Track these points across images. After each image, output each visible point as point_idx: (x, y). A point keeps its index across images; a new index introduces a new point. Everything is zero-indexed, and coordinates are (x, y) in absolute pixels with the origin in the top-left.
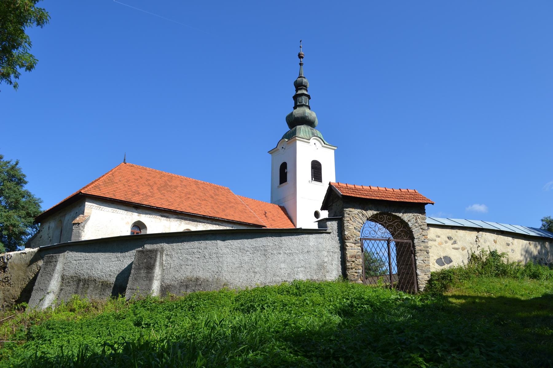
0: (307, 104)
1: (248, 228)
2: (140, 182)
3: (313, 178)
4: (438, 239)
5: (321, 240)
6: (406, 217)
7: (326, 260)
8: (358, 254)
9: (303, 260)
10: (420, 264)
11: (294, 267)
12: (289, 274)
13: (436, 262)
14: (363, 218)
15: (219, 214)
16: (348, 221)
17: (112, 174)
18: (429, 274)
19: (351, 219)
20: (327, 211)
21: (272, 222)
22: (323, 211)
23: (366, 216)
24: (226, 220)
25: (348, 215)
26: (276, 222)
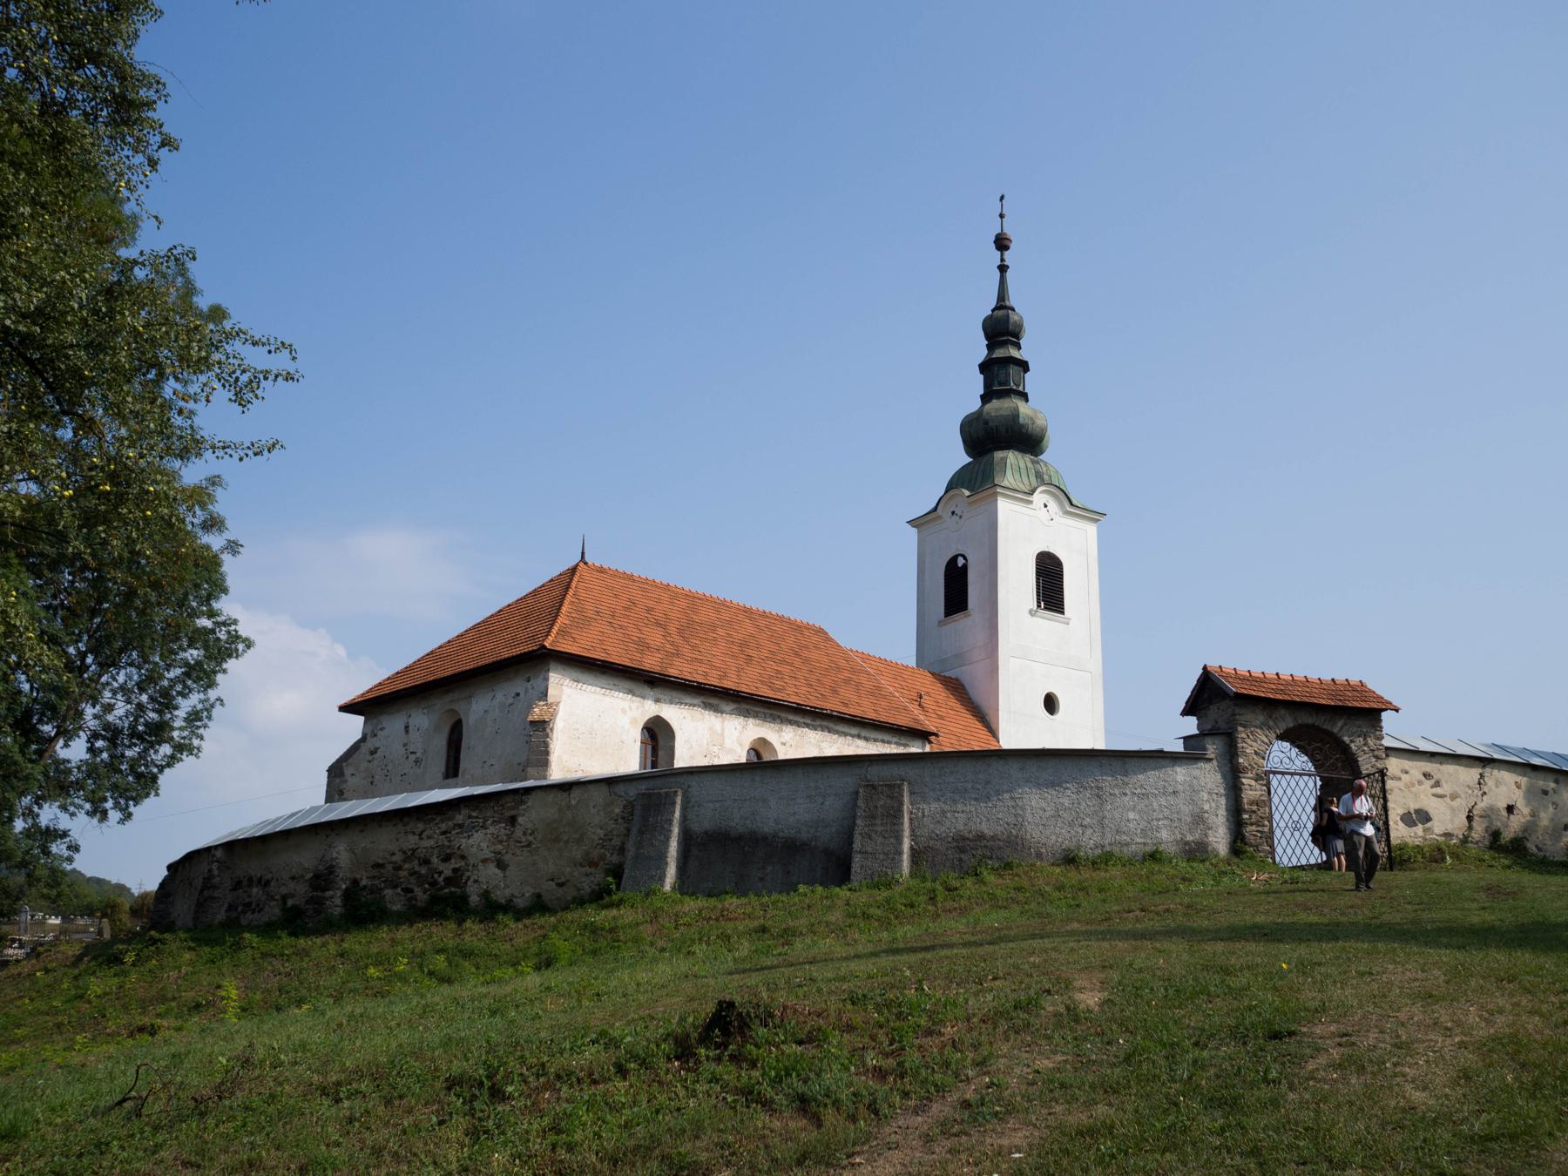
0: (1021, 389)
1: (905, 745)
4: (1404, 776)
5: (1196, 773)
6: (1337, 727)
7: (1206, 807)
8: (1263, 798)
13: (1401, 819)
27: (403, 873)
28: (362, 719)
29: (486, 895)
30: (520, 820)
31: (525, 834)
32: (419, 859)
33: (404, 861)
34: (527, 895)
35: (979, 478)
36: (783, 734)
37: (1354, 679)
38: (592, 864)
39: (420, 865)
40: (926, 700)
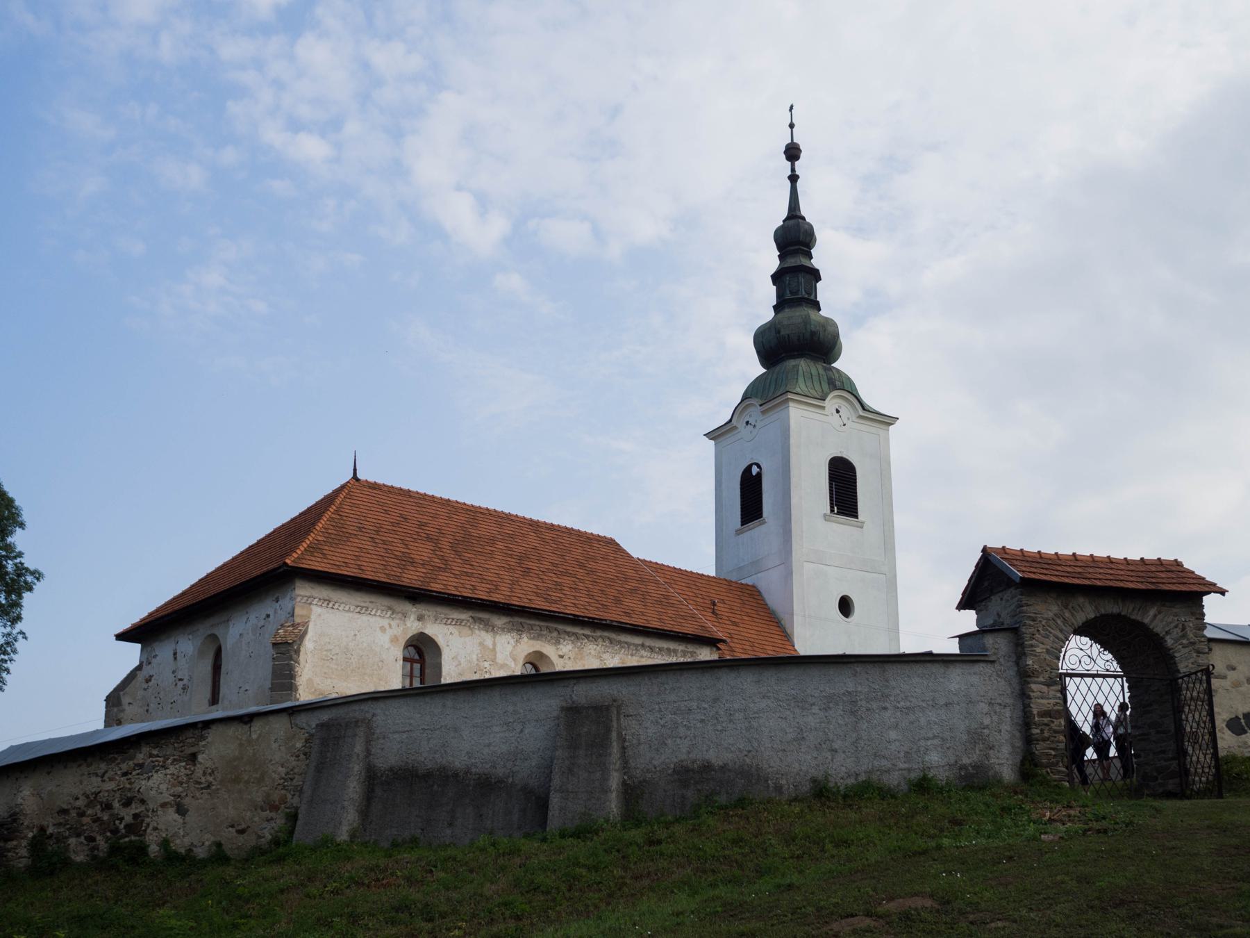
0: (812, 297)
2: (405, 531)
3: (836, 508)
7: (987, 721)
8: (1056, 708)
9: (935, 723)
11: (917, 738)
12: (908, 753)
13: (1227, 726)
14: (1064, 628)
15: (610, 611)
16: (1033, 635)
17: (337, 512)
19: (1038, 631)
20: (973, 612)
21: (732, 627)
22: (961, 611)
23: (1073, 624)
24: (628, 626)
25: (1032, 623)
26: (741, 629)
27: (85, 820)
28: (138, 646)
29: (165, 843)
30: (200, 758)
31: (204, 774)
32: (101, 803)
33: (88, 806)
34: (207, 843)
35: (773, 387)
36: (561, 646)
37: (1168, 556)
38: (274, 808)
39: (103, 810)
40: (720, 607)
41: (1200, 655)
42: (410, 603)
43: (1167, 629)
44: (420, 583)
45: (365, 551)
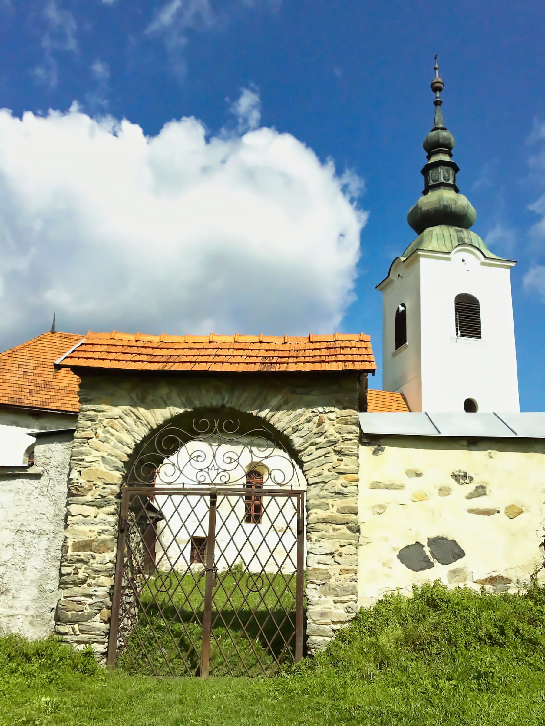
0: (451, 182)
4: (413, 483)
8: (103, 537)
10: (321, 566)
14: (135, 428)
18: (348, 601)
25: (89, 423)
41: (344, 458)
42: (33, 418)
43: (294, 424)
44: (39, 403)
45: (7, 381)
